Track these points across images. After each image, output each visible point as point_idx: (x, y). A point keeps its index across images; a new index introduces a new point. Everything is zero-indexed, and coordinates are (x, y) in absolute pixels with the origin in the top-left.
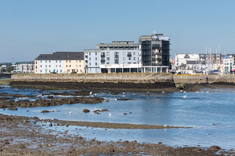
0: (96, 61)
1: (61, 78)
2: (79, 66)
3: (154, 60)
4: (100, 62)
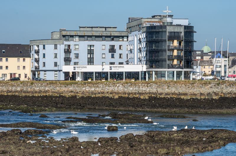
0: (56, 60)
1: (29, 89)
2: (21, 68)
3: (171, 58)
4: (63, 62)
